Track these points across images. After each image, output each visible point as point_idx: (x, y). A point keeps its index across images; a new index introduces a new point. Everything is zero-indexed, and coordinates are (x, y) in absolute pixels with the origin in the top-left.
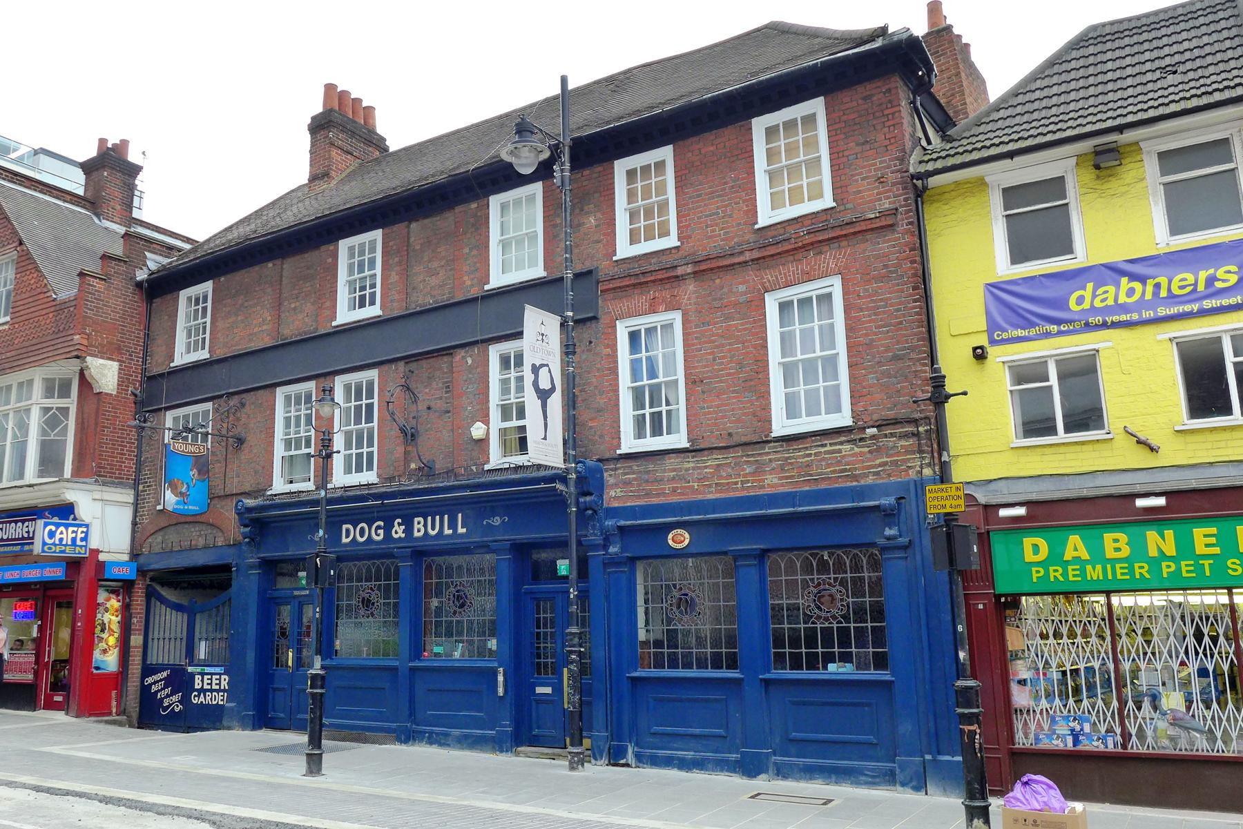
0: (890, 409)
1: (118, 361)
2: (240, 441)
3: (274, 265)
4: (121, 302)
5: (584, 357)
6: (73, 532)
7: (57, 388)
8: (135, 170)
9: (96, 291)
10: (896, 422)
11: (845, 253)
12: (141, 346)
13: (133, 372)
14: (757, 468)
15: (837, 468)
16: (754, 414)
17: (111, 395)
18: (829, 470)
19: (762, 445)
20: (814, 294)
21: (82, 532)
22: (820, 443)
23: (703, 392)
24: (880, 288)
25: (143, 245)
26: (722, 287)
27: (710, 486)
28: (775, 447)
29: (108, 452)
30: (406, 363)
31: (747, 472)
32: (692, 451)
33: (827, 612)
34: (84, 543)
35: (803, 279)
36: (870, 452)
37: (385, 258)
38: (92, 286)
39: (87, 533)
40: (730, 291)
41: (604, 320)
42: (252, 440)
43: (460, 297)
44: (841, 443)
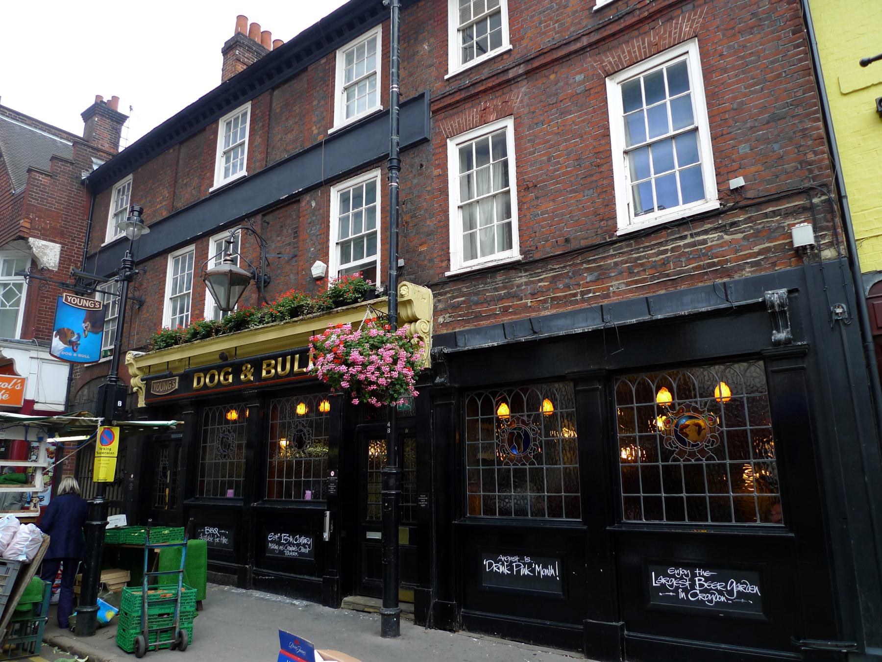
0: (770, 182)
2: (141, 303)
4: (66, 196)
5: (415, 181)
8: (122, 119)
9: (41, 184)
11: (702, 12)
12: (83, 233)
13: (75, 253)
14: (600, 275)
16: (596, 214)
18: (691, 266)
22: (678, 236)
23: (537, 198)
24: (749, 41)
25: (89, 151)
27: (545, 301)
29: (47, 318)
31: (588, 280)
33: (693, 446)
35: (650, 51)
36: (744, 238)
40: (567, 84)
41: (435, 141)
42: (149, 301)
43: (308, 146)
44: (706, 232)
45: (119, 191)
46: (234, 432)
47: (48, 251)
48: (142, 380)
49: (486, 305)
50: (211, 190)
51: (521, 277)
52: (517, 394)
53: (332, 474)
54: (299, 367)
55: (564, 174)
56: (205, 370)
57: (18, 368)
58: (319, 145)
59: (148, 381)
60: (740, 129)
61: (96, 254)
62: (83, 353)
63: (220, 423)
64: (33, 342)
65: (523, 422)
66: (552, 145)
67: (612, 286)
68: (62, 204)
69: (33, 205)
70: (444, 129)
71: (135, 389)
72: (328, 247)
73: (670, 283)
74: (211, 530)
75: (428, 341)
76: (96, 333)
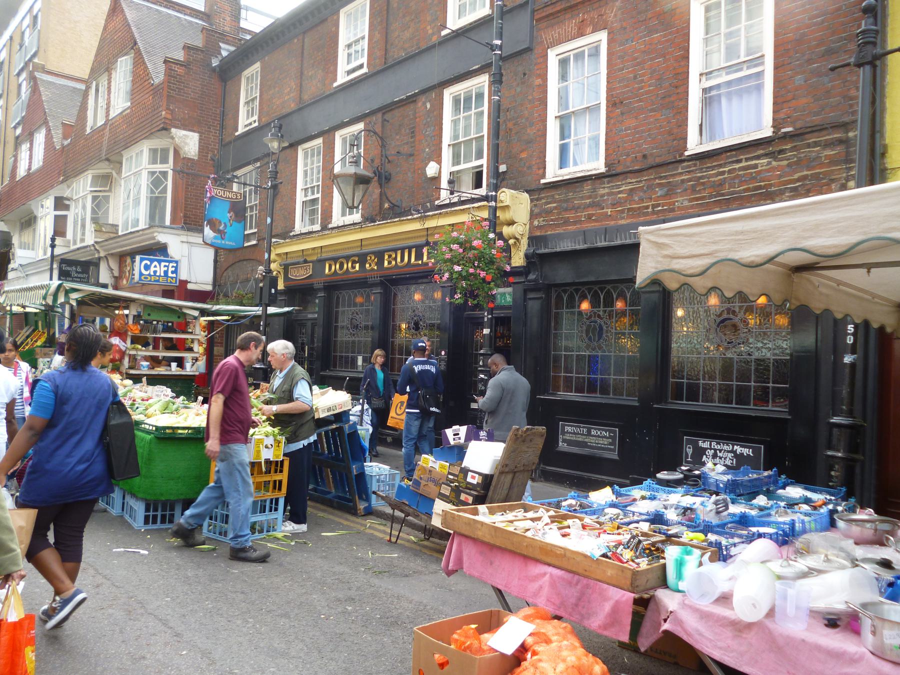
0: (817, 114)
1: (198, 132)
6: (165, 266)
7: (158, 155)
9: (177, 75)
10: (820, 129)
14: (668, 191)
15: (751, 186)
17: (193, 160)
19: (676, 165)
21: (173, 267)
25: (217, 37)
27: (622, 211)
28: (689, 167)
31: (659, 194)
34: (174, 275)
36: (789, 165)
38: (174, 71)
39: (176, 268)
44: (758, 157)
45: (248, 78)
46: (362, 314)
47: (188, 141)
48: (281, 265)
49: (574, 212)
50: (335, 85)
51: (604, 188)
52: (596, 292)
53: (443, 353)
54: (416, 260)
55: (647, 92)
56: (335, 260)
57: (171, 251)
58: (433, 46)
59: (286, 268)
60: (798, 60)
61: (230, 142)
62: (230, 241)
63: (349, 306)
64: (183, 227)
65: (599, 316)
66: (638, 63)
67: (677, 201)
68: (197, 93)
69: (172, 96)
70: (546, 38)
71: (275, 273)
72: (441, 149)
73: (724, 201)
75: (524, 242)
76: (240, 222)
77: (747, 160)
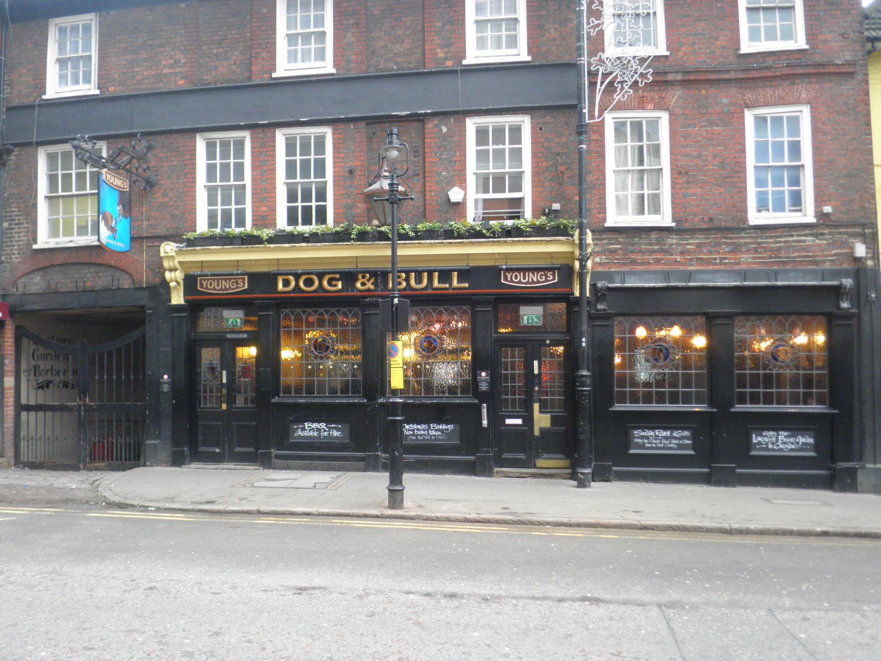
2: (150, 184)
3: (188, 6)
20: (785, 115)
26: (707, 98)
27: (691, 260)
30: (367, 124)
32: (679, 230)
37: (337, 18)
44: (806, 235)
74: (314, 425)
77: (798, 236)
